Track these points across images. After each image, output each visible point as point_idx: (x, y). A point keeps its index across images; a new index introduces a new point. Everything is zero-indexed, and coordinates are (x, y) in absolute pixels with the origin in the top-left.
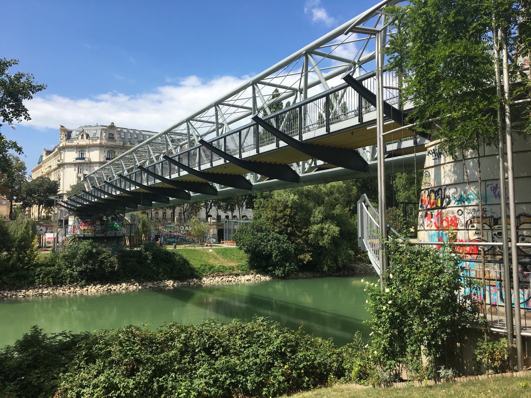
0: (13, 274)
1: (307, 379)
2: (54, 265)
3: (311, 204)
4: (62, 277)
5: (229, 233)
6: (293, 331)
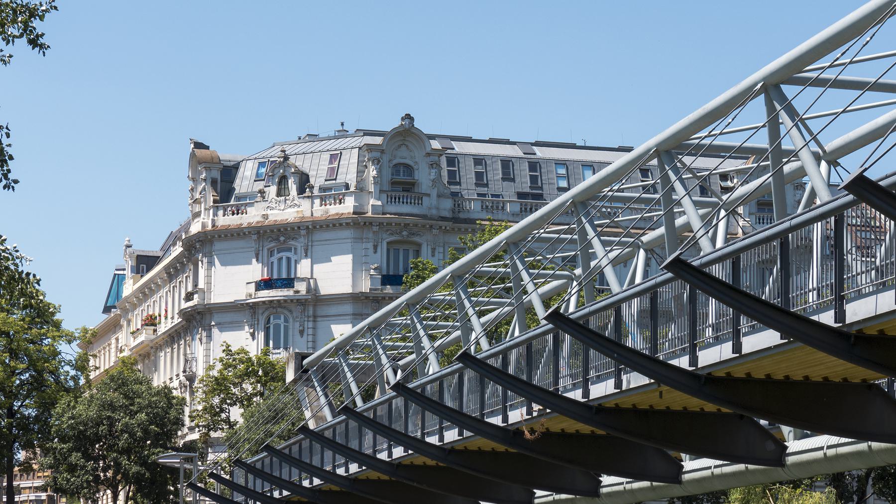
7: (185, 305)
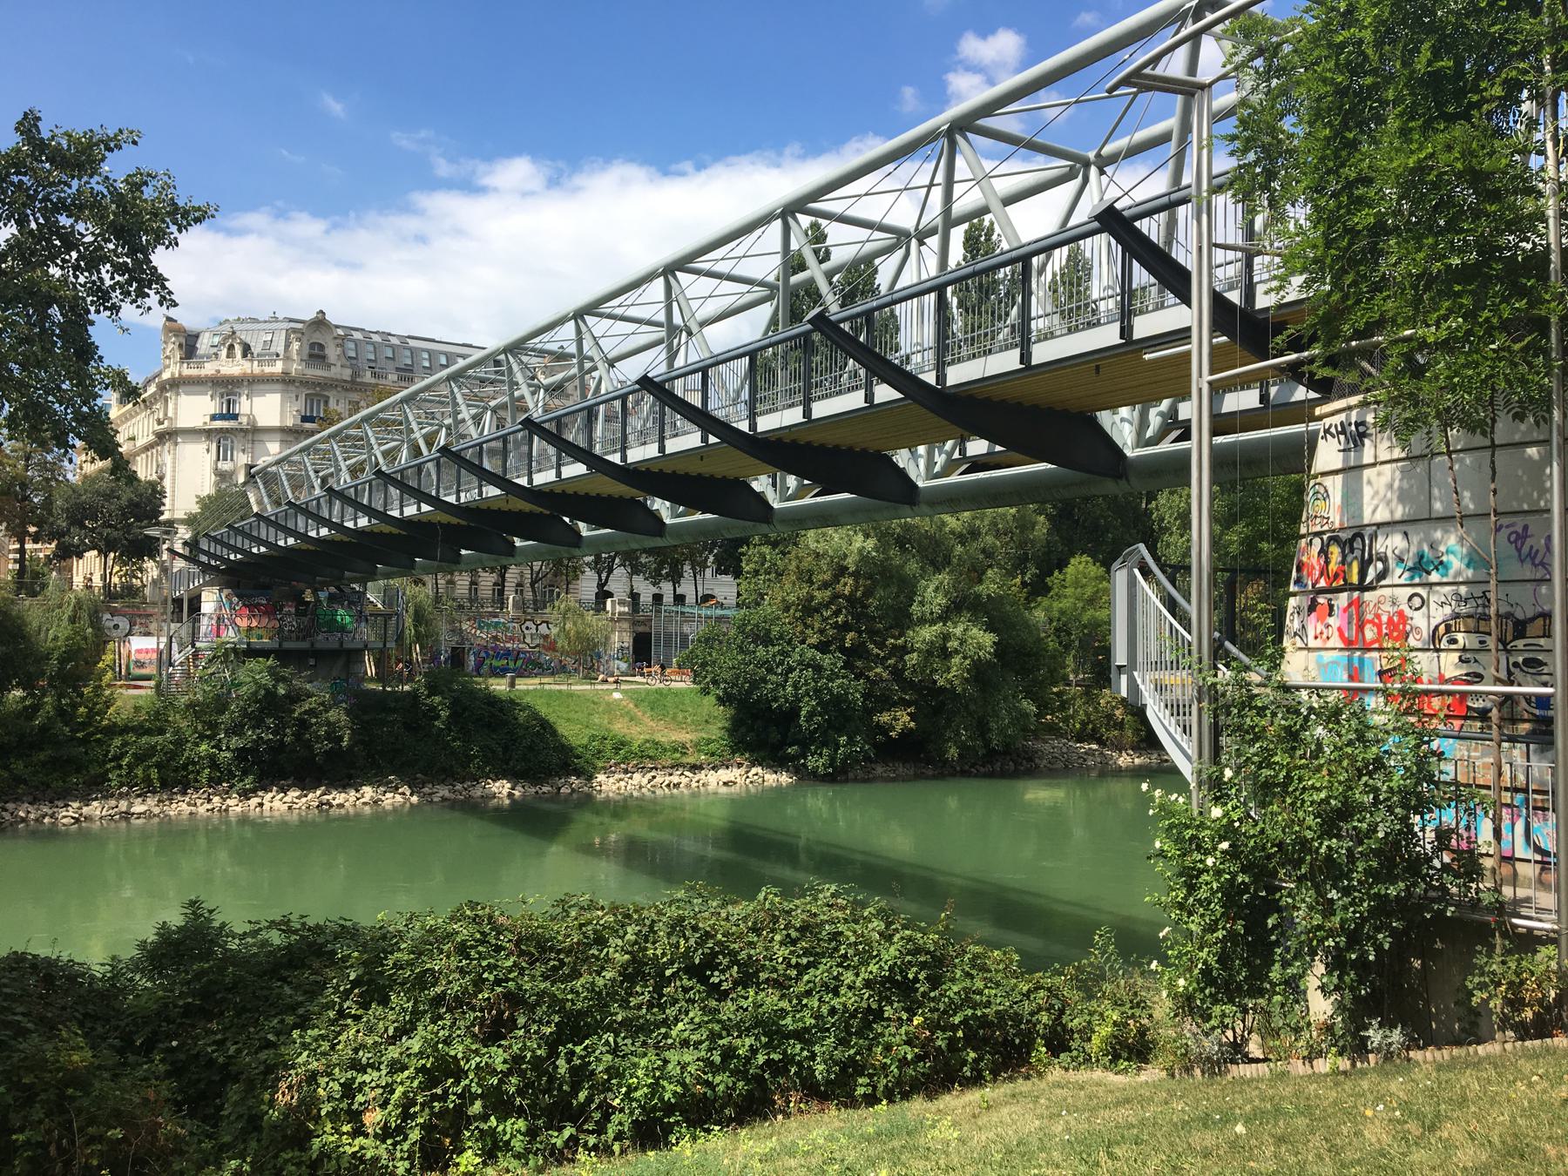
0: (42, 756)
1: (973, 1055)
2: (161, 732)
3: (913, 567)
4: (185, 767)
5: (668, 644)
6: (923, 924)
7: (157, 427)
